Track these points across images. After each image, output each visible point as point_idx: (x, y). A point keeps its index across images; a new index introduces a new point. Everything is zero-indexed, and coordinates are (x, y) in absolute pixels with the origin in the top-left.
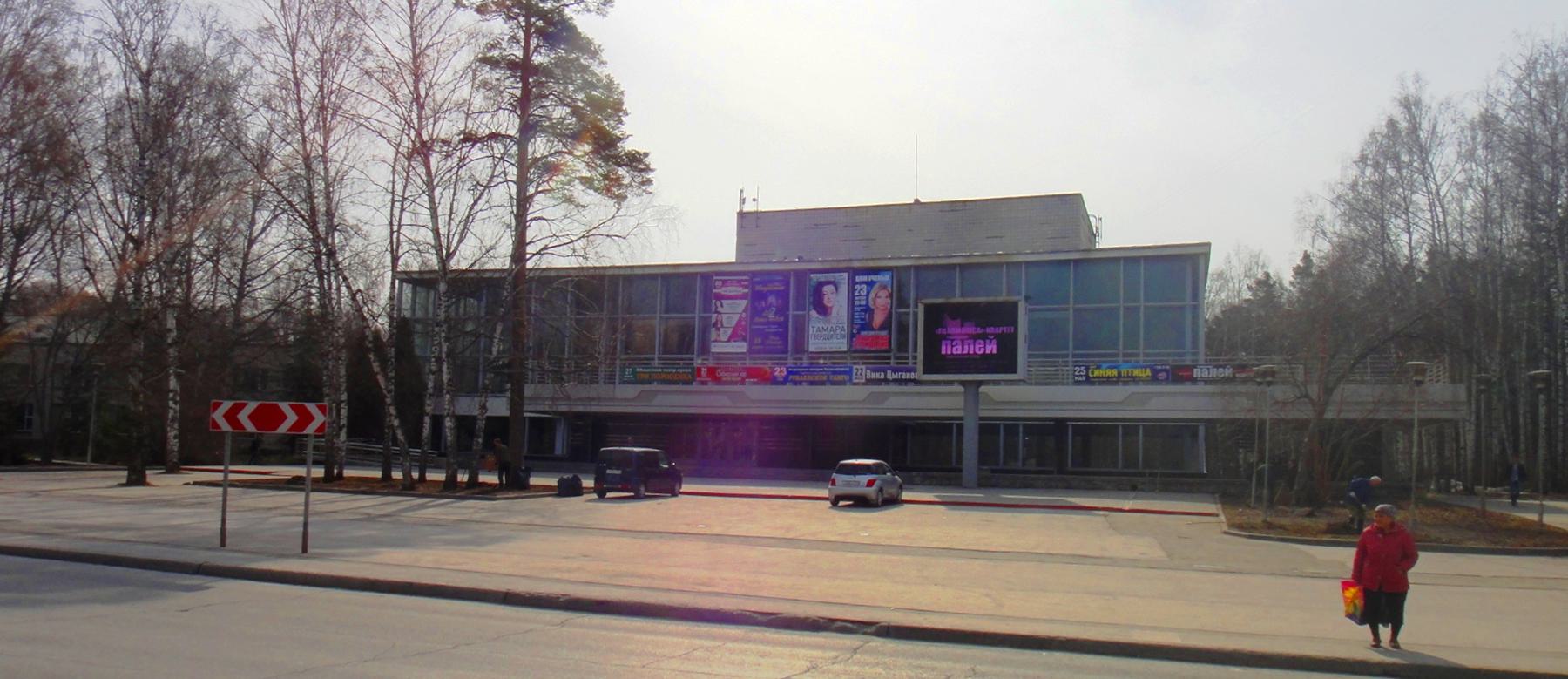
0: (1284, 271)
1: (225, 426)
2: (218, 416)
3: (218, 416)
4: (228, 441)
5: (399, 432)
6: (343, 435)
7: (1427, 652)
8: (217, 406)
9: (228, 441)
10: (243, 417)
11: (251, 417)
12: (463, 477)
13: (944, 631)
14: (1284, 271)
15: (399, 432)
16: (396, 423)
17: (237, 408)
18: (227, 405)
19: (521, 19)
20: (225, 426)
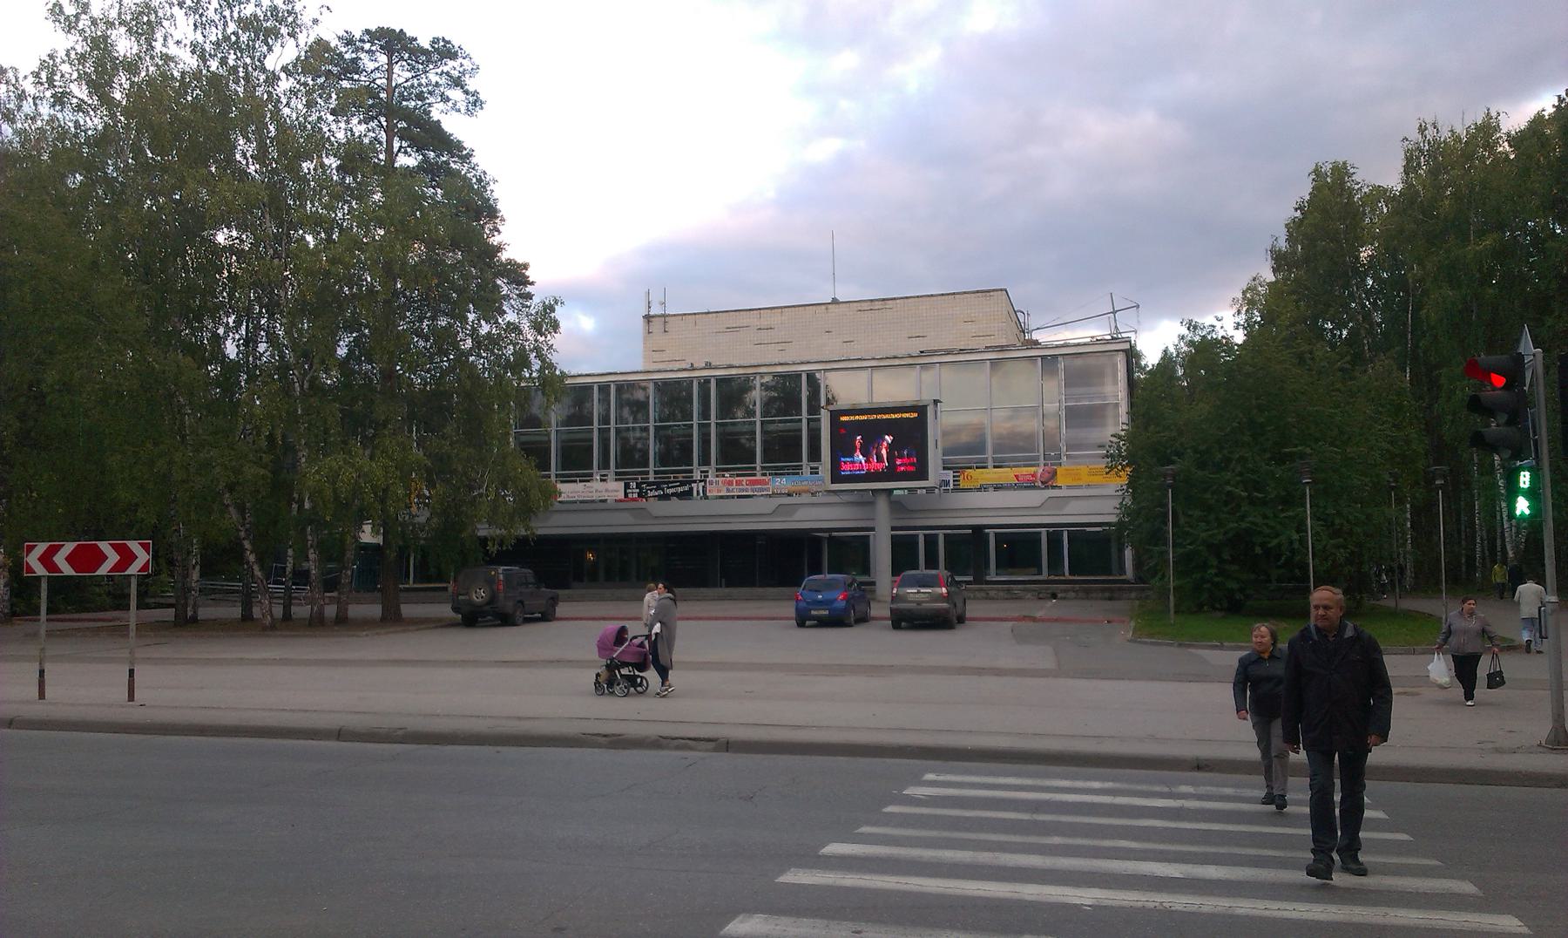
0: (1461, 131)
1: (40, 570)
2: (142, 557)
3: (142, 557)
4: (44, 585)
5: (256, 567)
6: (195, 575)
7: (1039, 655)
8: (31, 549)
9: (44, 585)
10: (113, 557)
11: (69, 559)
12: (331, 611)
13: (747, 752)
14: (1461, 131)
15: (256, 567)
16: (252, 558)
17: (53, 550)
18: (41, 547)
19: (383, 119)
20: (40, 570)
